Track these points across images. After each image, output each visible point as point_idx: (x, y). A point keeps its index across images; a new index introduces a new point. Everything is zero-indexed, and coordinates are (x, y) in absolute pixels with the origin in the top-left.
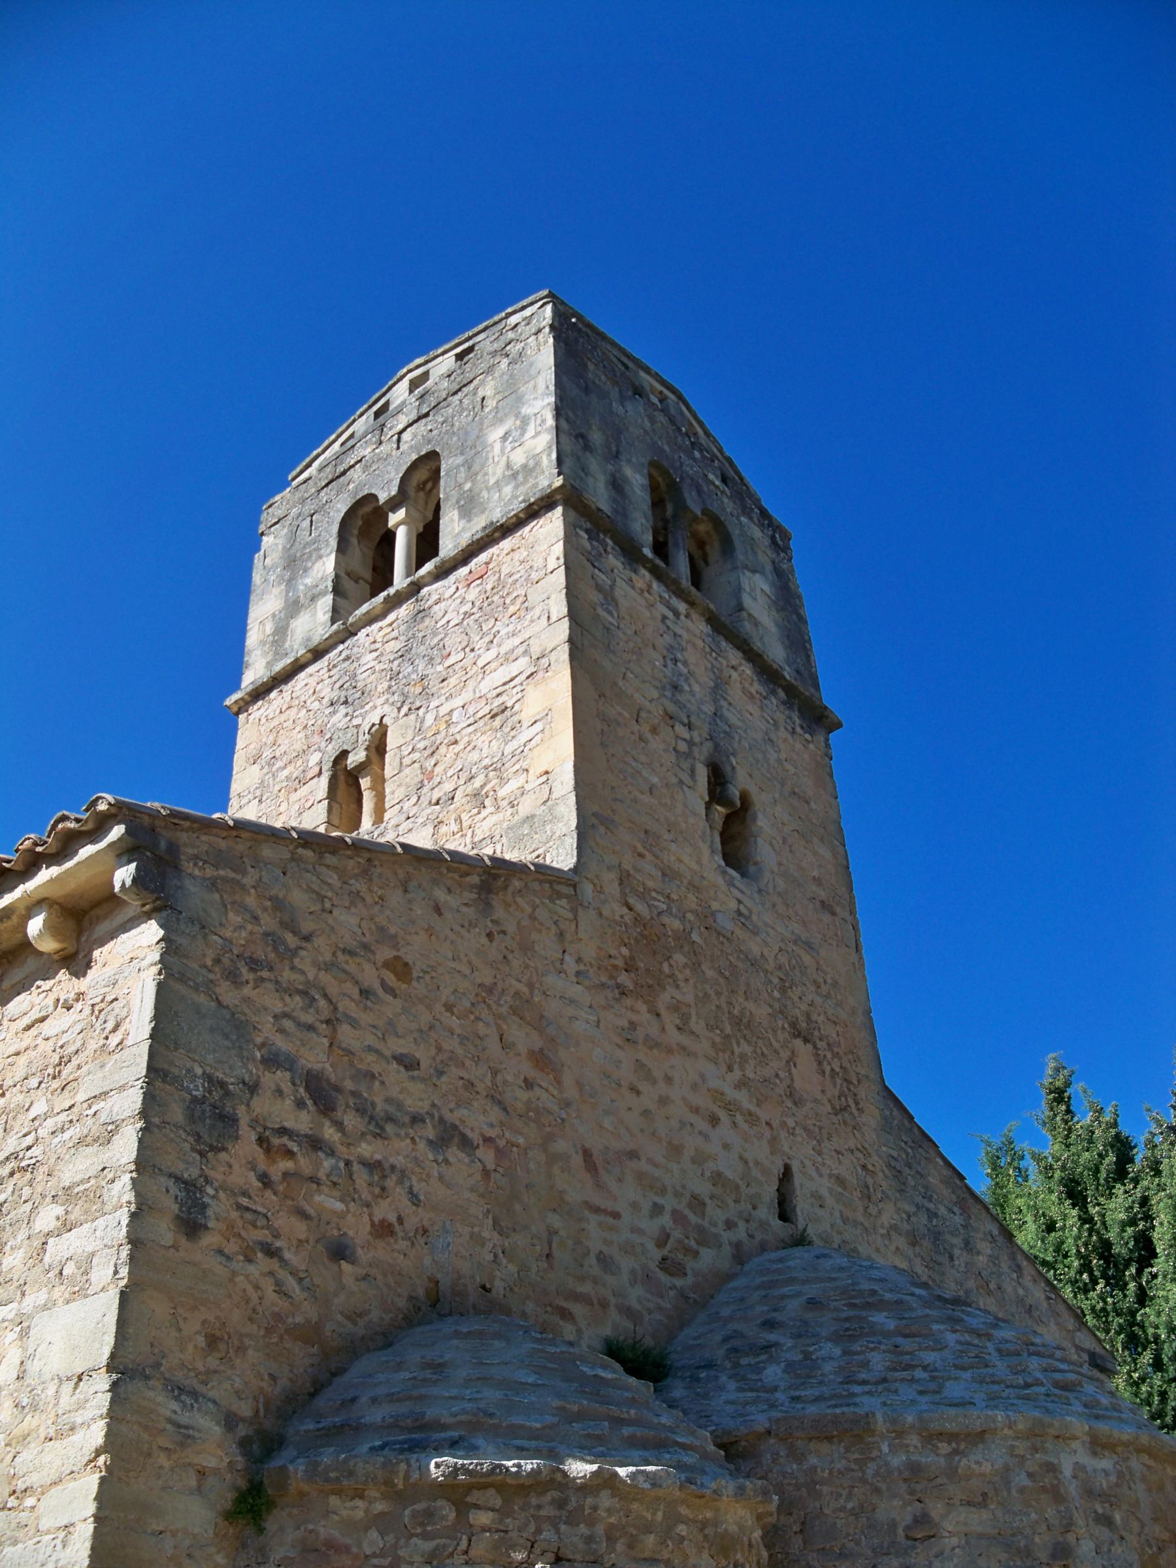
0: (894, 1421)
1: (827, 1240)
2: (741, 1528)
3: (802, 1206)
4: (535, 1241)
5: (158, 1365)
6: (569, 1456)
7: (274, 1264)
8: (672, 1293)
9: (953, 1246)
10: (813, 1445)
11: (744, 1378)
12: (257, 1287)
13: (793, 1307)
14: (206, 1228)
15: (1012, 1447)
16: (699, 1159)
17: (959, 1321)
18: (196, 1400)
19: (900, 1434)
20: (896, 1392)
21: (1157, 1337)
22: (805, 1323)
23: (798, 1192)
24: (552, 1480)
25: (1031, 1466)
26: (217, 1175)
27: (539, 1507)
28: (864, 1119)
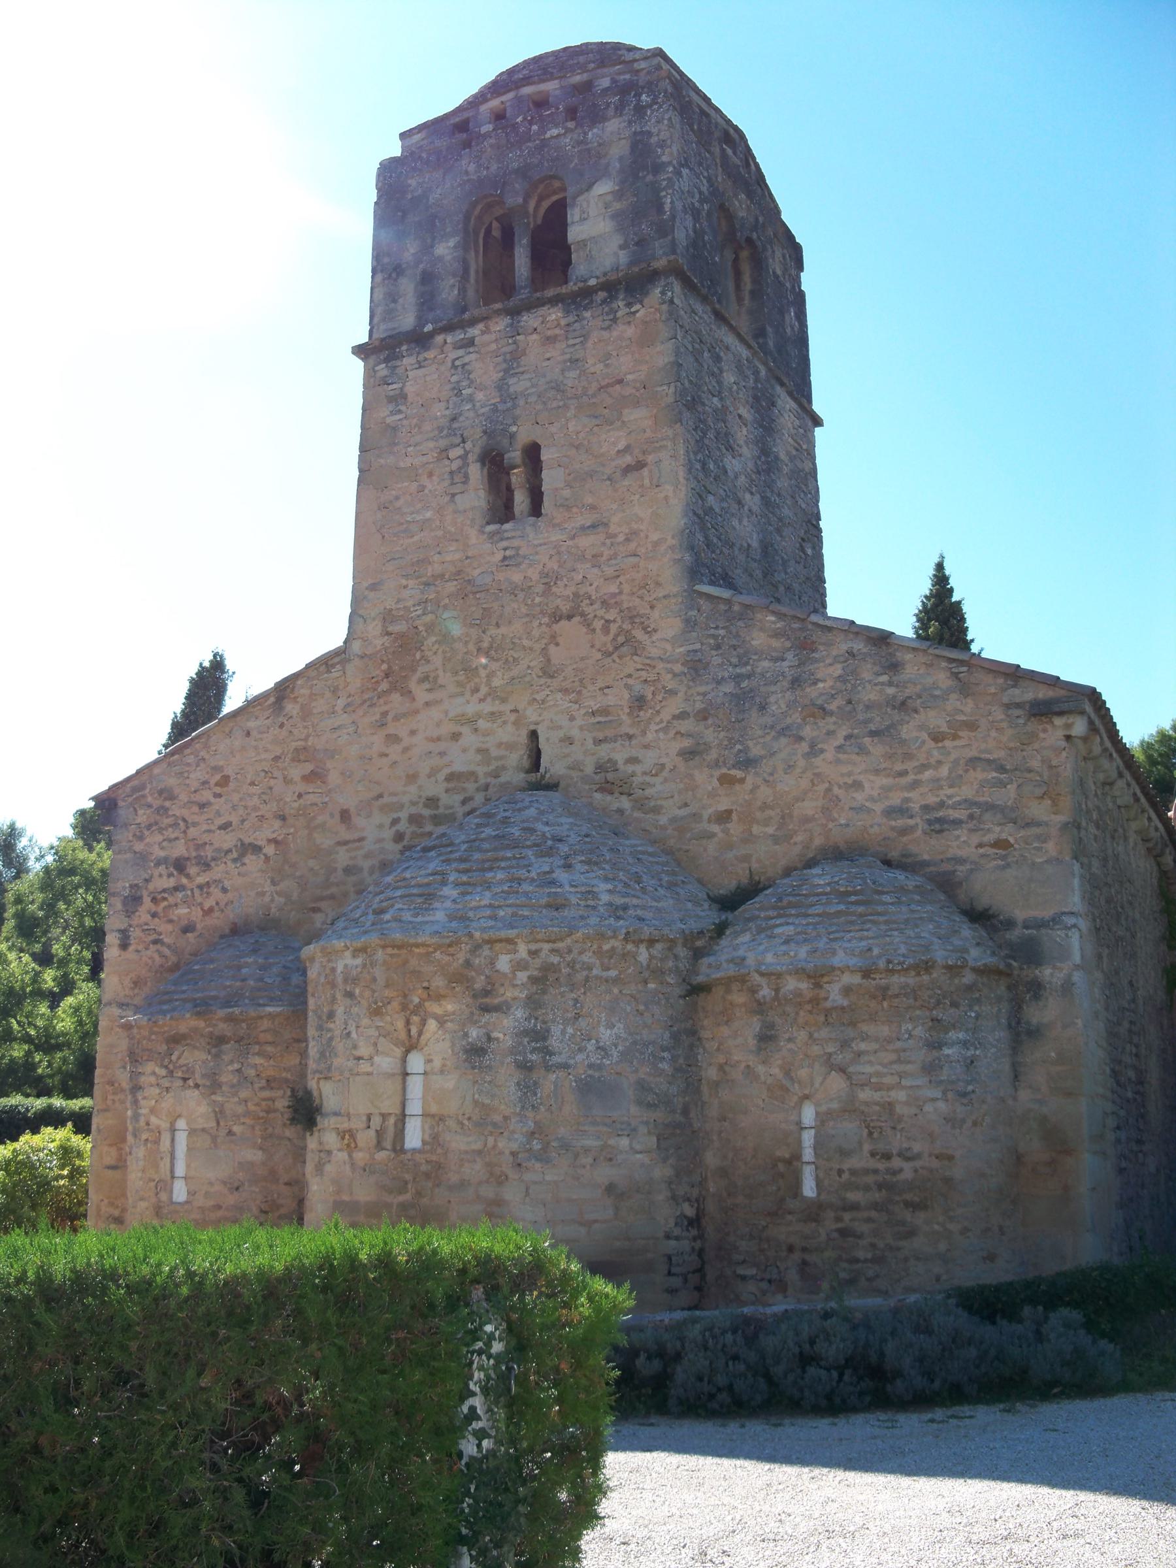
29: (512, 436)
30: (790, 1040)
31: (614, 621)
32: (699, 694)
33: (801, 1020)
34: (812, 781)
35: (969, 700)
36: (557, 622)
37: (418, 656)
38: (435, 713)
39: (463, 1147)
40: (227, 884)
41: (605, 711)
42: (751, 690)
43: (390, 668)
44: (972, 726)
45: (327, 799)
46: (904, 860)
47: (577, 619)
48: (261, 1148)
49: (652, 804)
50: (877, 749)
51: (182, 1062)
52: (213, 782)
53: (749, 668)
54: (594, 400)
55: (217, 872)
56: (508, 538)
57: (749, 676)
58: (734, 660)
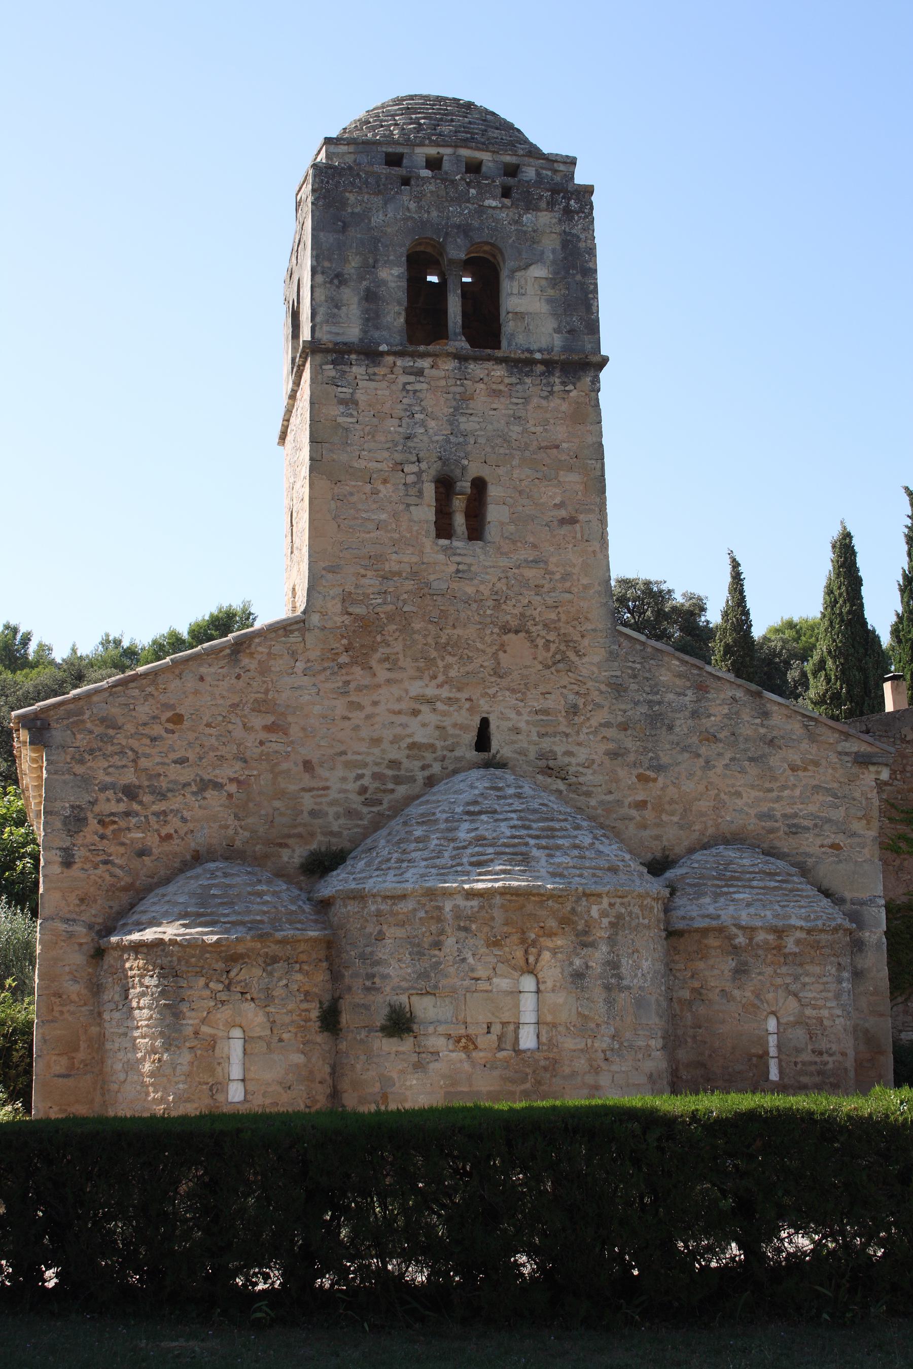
25: (427, 908)
29: (464, 468)
30: (760, 974)
31: (554, 642)
32: (620, 710)
33: (768, 961)
34: (706, 787)
35: (814, 745)
36: (506, 634)
37: (379, 638)
38: (396, 690)
39: (572, 1047)
40: (186, 814)
41: (546, 712)
42: (660, 714)
43: (350, 643)
44: (816, 764)
45: (289, 749)
46: (771, 850)
47: (522, 635)
48: (302, 1053)
49: (585, 789)
50: (753, 770)
51: (240, 978)
52: (164, 718)
53: (659, 697)
54: (535, 456)
55: (175, 802)
56: (460, 555)
57: (659, 703)
58: (647, 689)
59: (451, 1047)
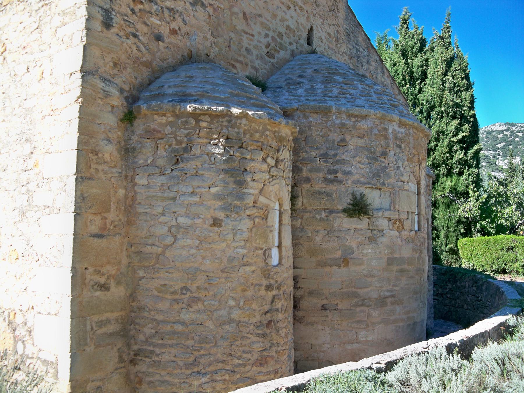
0: (338, 110)
1: (322, 53)
2: (287, 135)
3: (315, 40)
4: (225, 41)
5: (97, 71)
6: (233, 107)
7: (136, 40)
8: (270, 64)
9: (363, 62)
10: (311, 115)
11: (291, 92)
12: (130, 48)
13: (309, 71)
14: (113, 26)
15: (375, 122)
16: (282, 20)
17: (363, 81)
18: (110, 83)
19: (340, 114)
20: (340, 101)
21: (422, 104)
22: (313, 77)
23: (314, 36)
24: (227, 114)
26: (116, 8)
27: (222, 122)
28: (339, 15)
59: (391, 227)
